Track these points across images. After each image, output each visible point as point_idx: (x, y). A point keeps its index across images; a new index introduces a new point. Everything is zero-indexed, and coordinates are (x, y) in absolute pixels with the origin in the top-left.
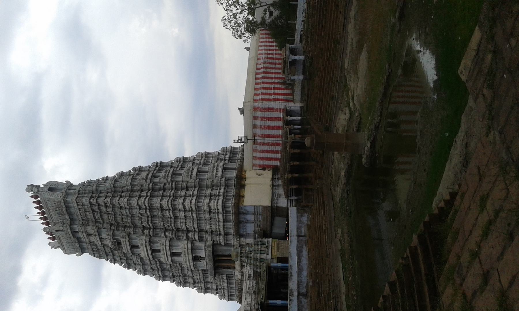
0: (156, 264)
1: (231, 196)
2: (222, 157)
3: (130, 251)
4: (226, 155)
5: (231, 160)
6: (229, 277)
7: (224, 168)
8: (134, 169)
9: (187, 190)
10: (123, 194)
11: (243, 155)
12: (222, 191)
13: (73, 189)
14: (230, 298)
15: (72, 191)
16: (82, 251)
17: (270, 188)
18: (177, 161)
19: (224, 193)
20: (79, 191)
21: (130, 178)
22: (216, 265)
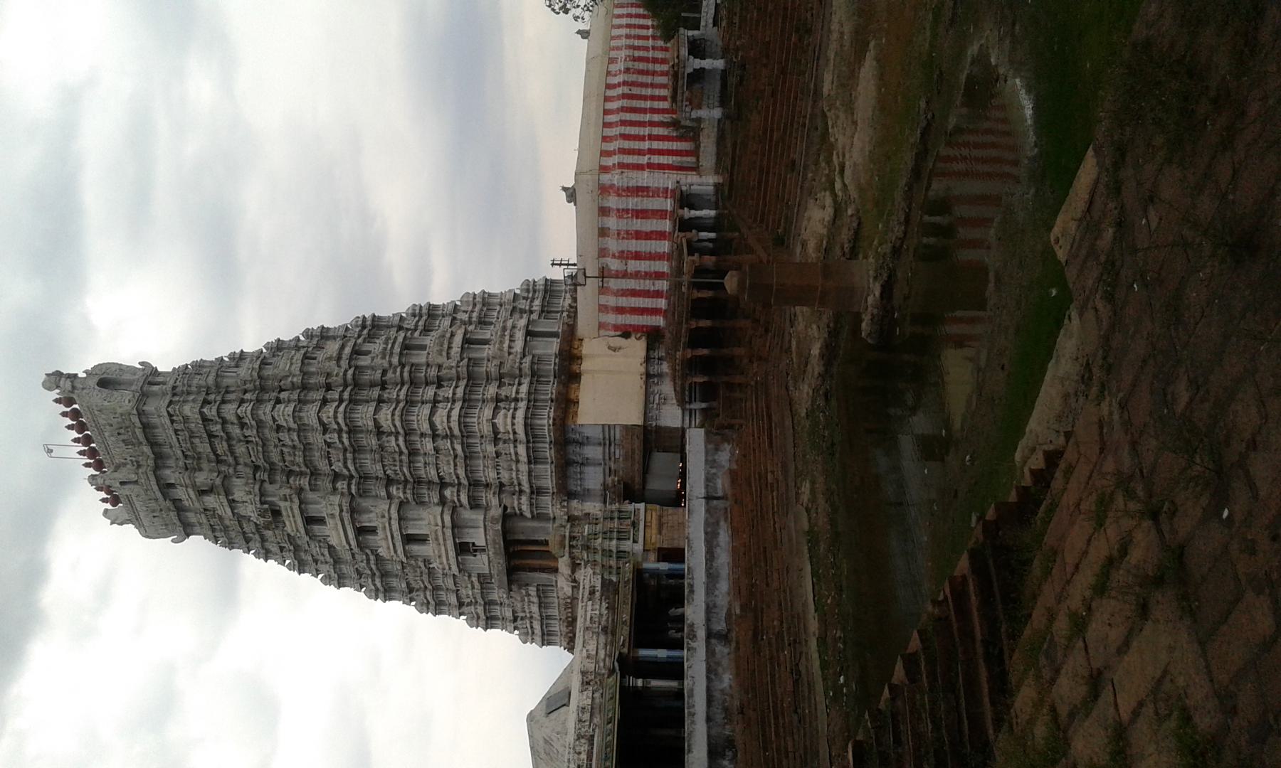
0: (368, 560)
1: (546, 401)
2: (523, 304)
5: (545, 311)
7: (529, 334)
8: (309, 334)
9: (439, 386)
10: (284, 395)
11: (575, 300)
12: (524, 389)
13: (158, 384)
14: (546, 639)
15: (155, 388)
16: (187, 530)
17: (642, 383)
18: (414, 315)
19: (529, 393)
20: (174, 388)
21: (299, 356)
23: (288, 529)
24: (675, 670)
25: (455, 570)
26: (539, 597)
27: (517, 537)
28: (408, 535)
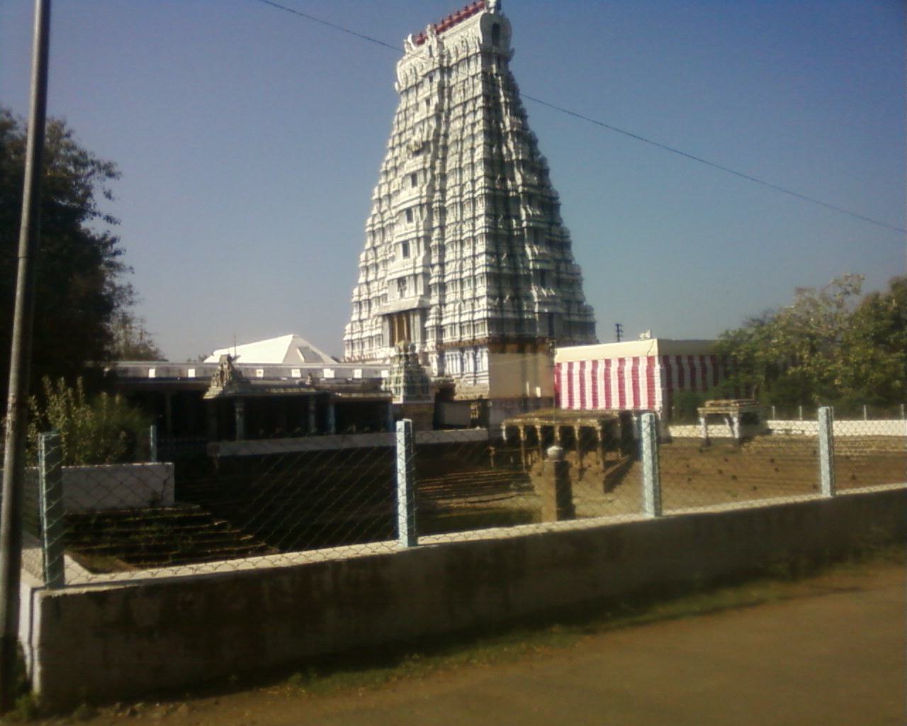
0: (391, 218)
2: (574, 309)
3: (408, 172)
4: (580, 315)
6: (379, 339)
12: (510, 315)
22: (404, 315)
23: (409, 162)
24: (322, 429)
25: (389, 278)
26: (376, 336)
27: (412, 317)
28: (409, 244)
